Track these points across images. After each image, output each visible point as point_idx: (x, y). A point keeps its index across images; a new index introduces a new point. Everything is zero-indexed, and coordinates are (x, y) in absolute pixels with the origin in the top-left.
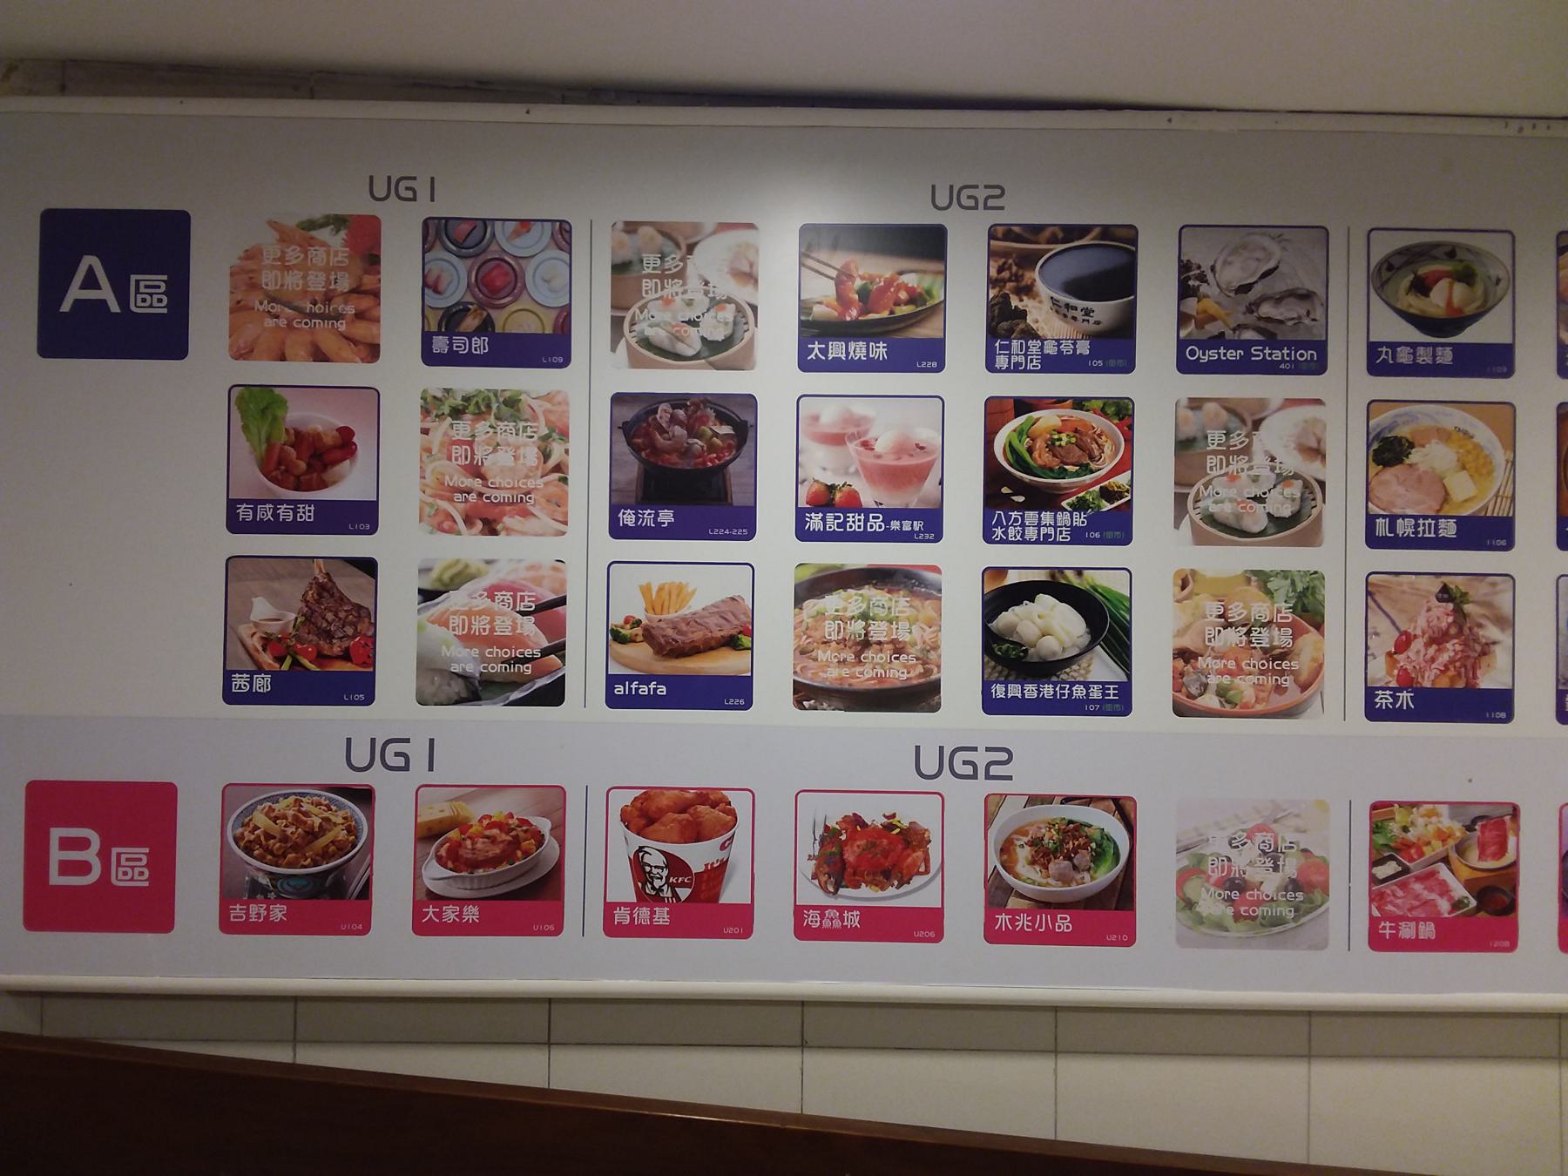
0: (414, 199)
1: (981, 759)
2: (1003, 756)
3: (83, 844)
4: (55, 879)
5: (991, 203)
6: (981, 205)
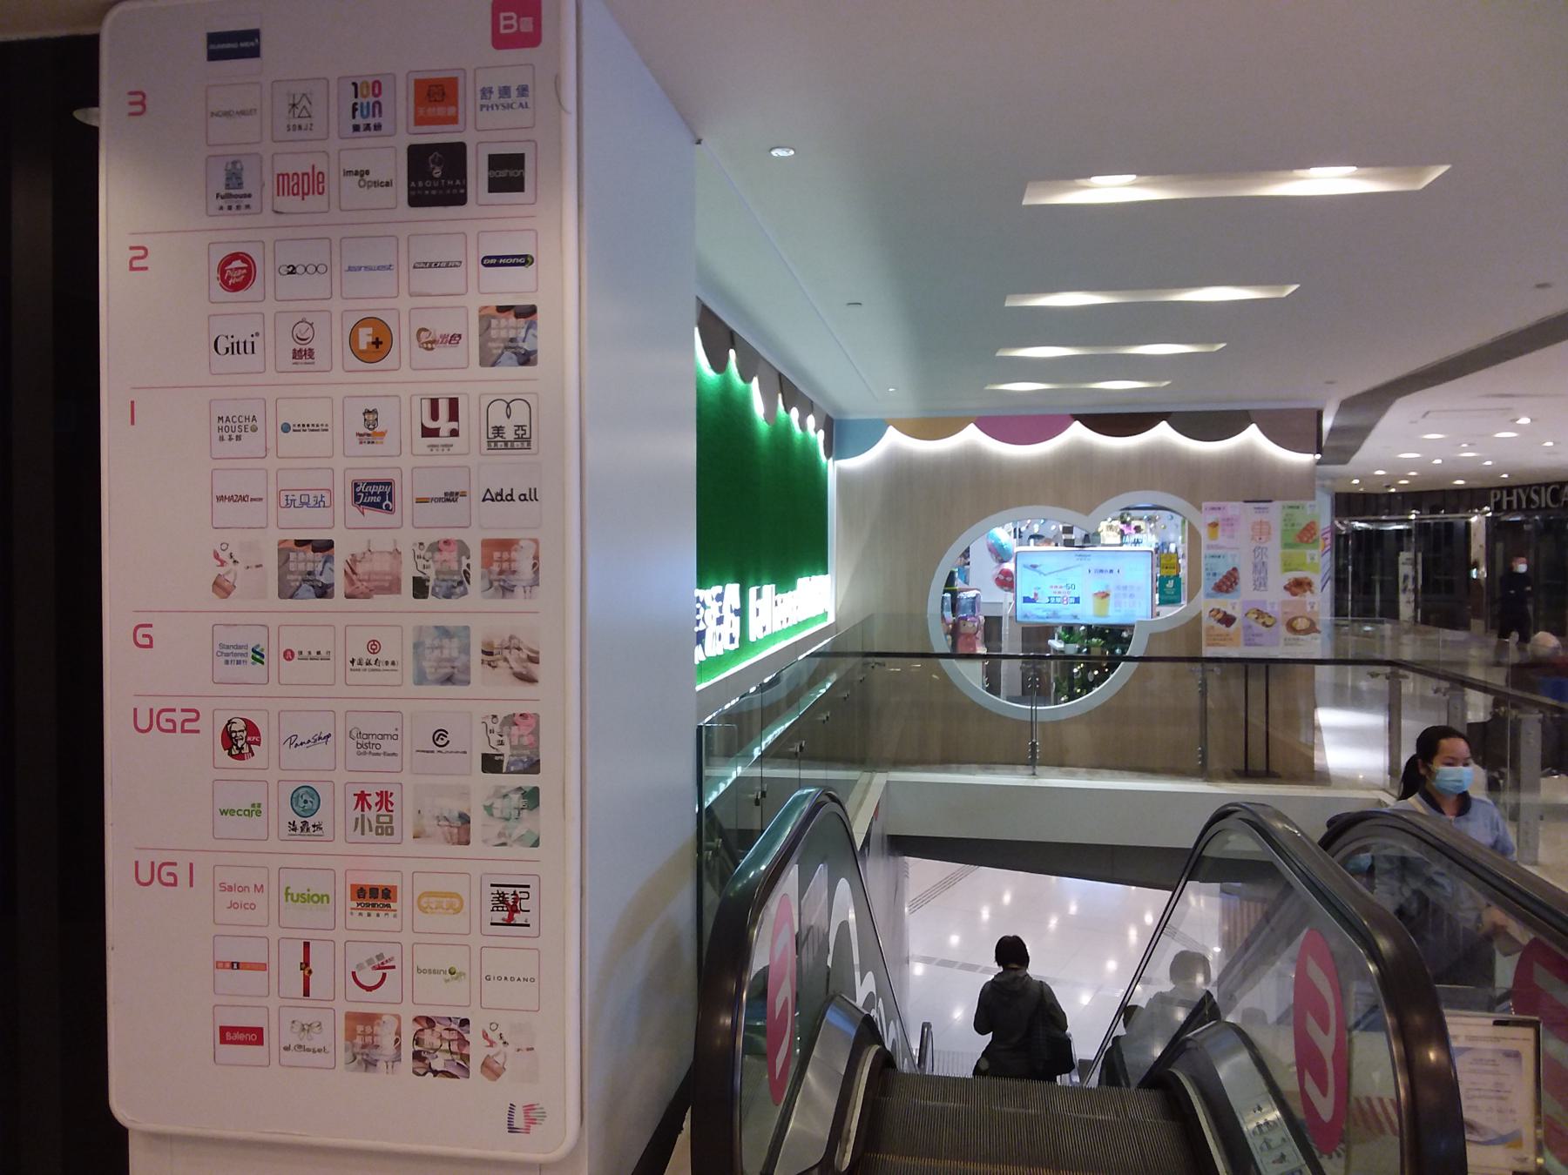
0: (150, 646)
1: (178, 717)
2: (193, 715)
3: (506, 27)
4: (502, 31)
5: (188, 726)
6: (179, 728)
